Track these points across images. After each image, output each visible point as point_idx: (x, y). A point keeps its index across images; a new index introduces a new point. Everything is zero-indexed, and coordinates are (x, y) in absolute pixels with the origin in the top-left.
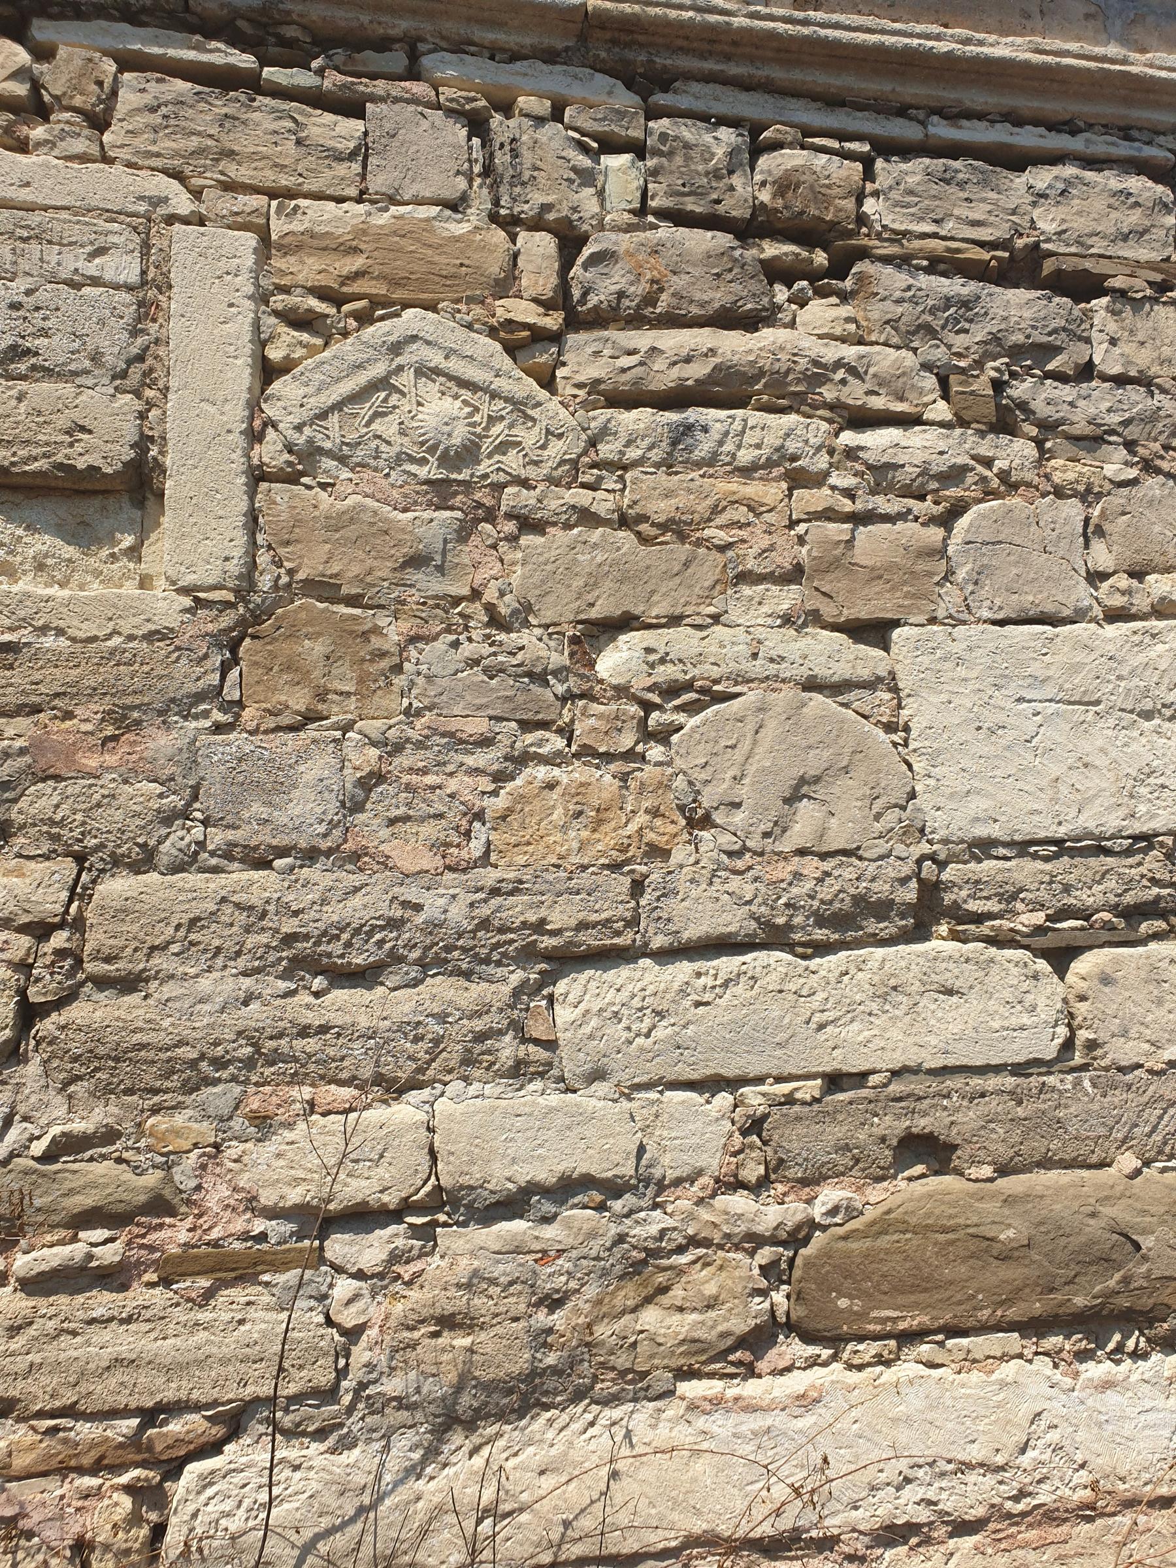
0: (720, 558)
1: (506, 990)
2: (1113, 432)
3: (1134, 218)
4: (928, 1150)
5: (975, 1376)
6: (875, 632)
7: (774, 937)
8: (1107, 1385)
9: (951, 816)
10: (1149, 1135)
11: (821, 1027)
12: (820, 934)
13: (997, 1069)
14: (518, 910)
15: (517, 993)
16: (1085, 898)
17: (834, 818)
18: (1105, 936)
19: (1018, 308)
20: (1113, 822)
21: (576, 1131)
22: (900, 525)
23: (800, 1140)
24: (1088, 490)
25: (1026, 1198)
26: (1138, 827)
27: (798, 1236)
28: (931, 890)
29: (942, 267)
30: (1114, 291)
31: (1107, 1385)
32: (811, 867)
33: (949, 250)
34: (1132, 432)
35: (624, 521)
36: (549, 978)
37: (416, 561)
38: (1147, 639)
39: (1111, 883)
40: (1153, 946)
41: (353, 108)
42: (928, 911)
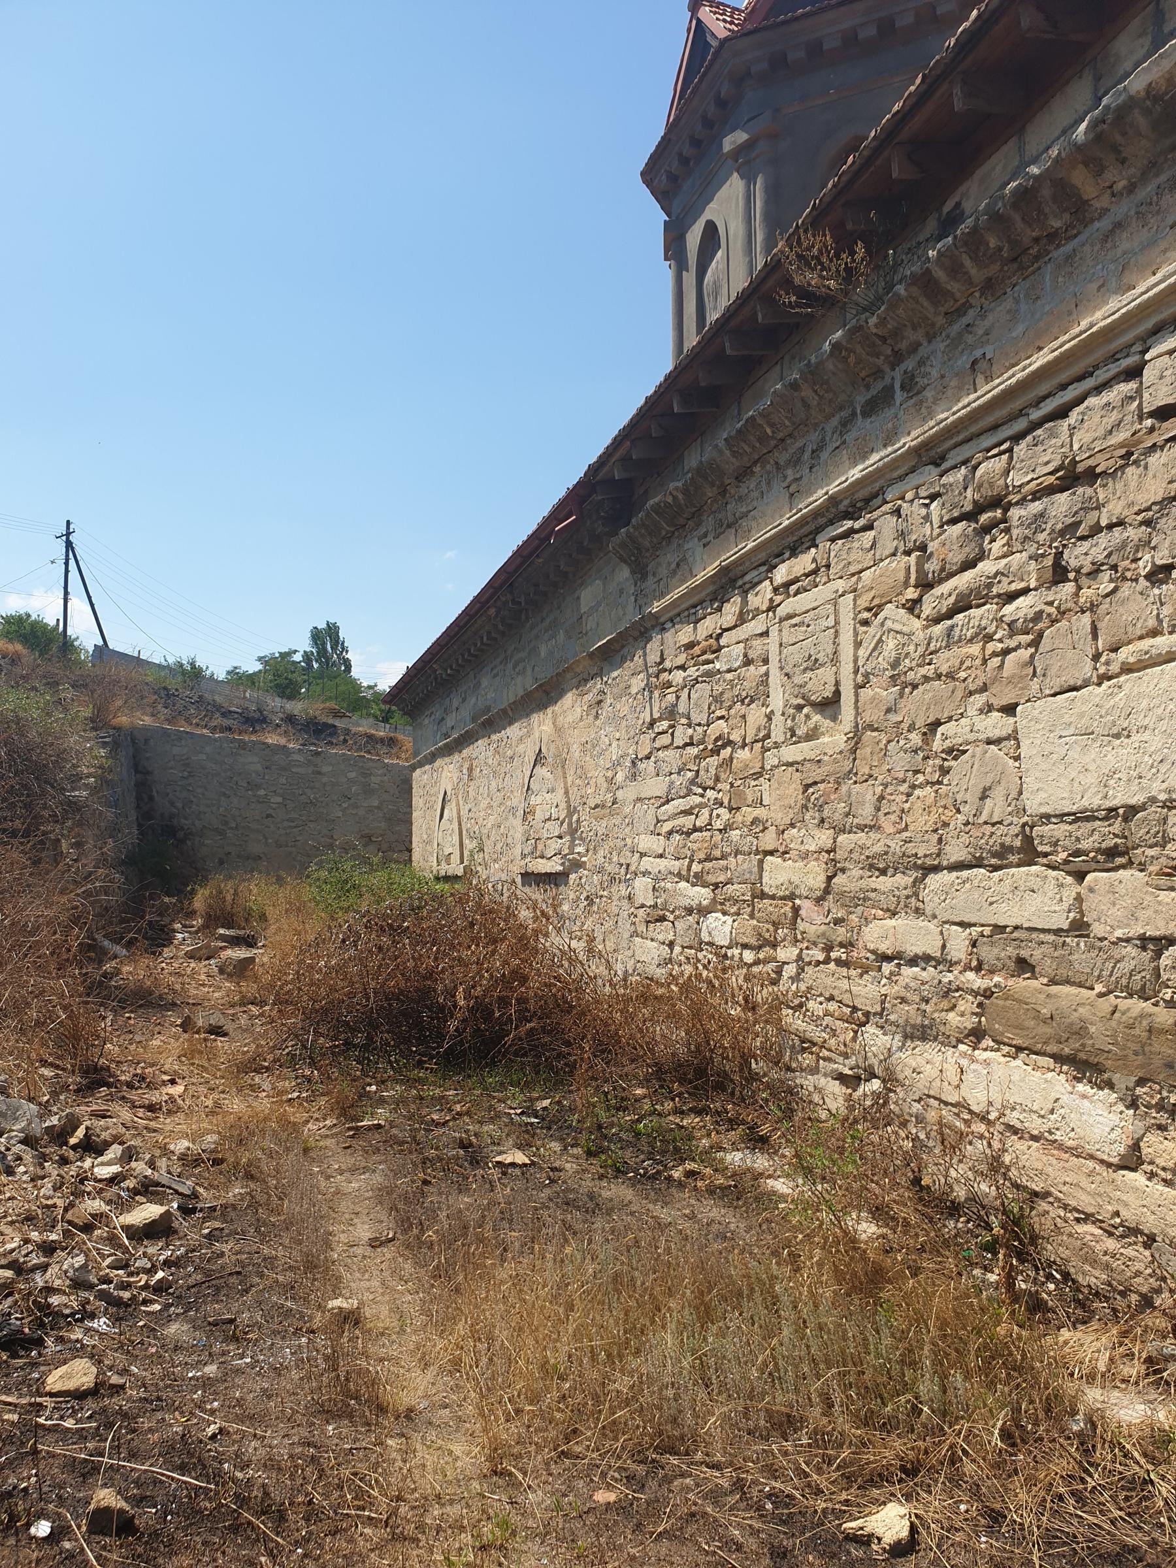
0: (963, 685)
1: (911, 880)
2: (1103, 564)
3: (1114, 416)
4: (1023, 966)
5: (1038, 1074)
6: (1010, 710)
7: (978, 863)
8: (1084, 1096)
9: (1034, 804)
10: (1111, 976)
11: (991, 904)
12: (993, 861)
13: (1048, 931)
14: (910, 849)
15: (914, 882)
16: (1085, 845)
17: (995, 807)
18: (1094, 865)
19: (1062, 505)
20: (1096, 802)
21: (916, 935)
22: (1019, 651)
23: (988, 953)
24: (1092, 604)
25: (1056, 996)
26: (1109, 804)
27: (988, 994)
28: (1028, 840)
29: (1038, 495)
30: (1100, 474)
31: (1084, 1096)
32: (988, 829)
33: (1038, 485)
34: (1114, 559)
35: (939, 677)
36: (925, 876)
37: (888, 711)
38: (1116, 690)
39: (1096, 837)
40: (1121, 872)
41: (869, 527)
42: (1029, 853)
